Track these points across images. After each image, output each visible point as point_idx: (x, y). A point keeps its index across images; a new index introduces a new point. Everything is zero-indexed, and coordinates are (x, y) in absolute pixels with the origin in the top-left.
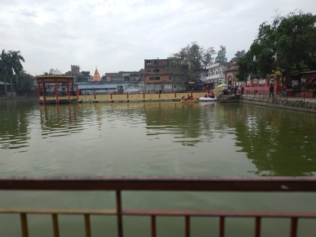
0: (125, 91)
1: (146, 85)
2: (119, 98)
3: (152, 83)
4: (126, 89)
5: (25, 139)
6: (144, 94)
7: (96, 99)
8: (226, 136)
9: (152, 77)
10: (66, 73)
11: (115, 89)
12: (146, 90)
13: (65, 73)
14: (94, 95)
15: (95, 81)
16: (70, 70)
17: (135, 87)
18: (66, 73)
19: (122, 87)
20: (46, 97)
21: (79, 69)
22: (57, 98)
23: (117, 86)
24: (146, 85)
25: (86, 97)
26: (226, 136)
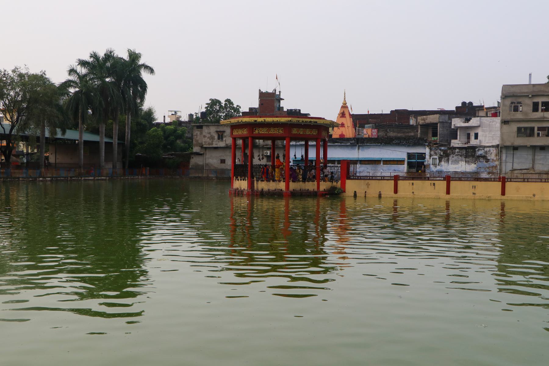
0: (433, 168)
1: (504, 151)
2: (474, 194)
3: (525, 147)
4: (435, 165)
5: (133, 295)
6: (503, 181)
7: (451, 194)
8: (19, 293)
9: (526, 128)
10: (457, 108)
11: (400, 162)
12: (504, 170)
13: (454, 109)
14: (393, 181)
15: (338, 137)
16: (256, 105)
17: (464, 159)
18: (457, 108)
19: (422, 156)
20: (255, 182)
21: (280, 102)
22: (287, 186)
23: (408, 153)
24: (504, 151)
25: (368, 185)
26: (19, 293)
